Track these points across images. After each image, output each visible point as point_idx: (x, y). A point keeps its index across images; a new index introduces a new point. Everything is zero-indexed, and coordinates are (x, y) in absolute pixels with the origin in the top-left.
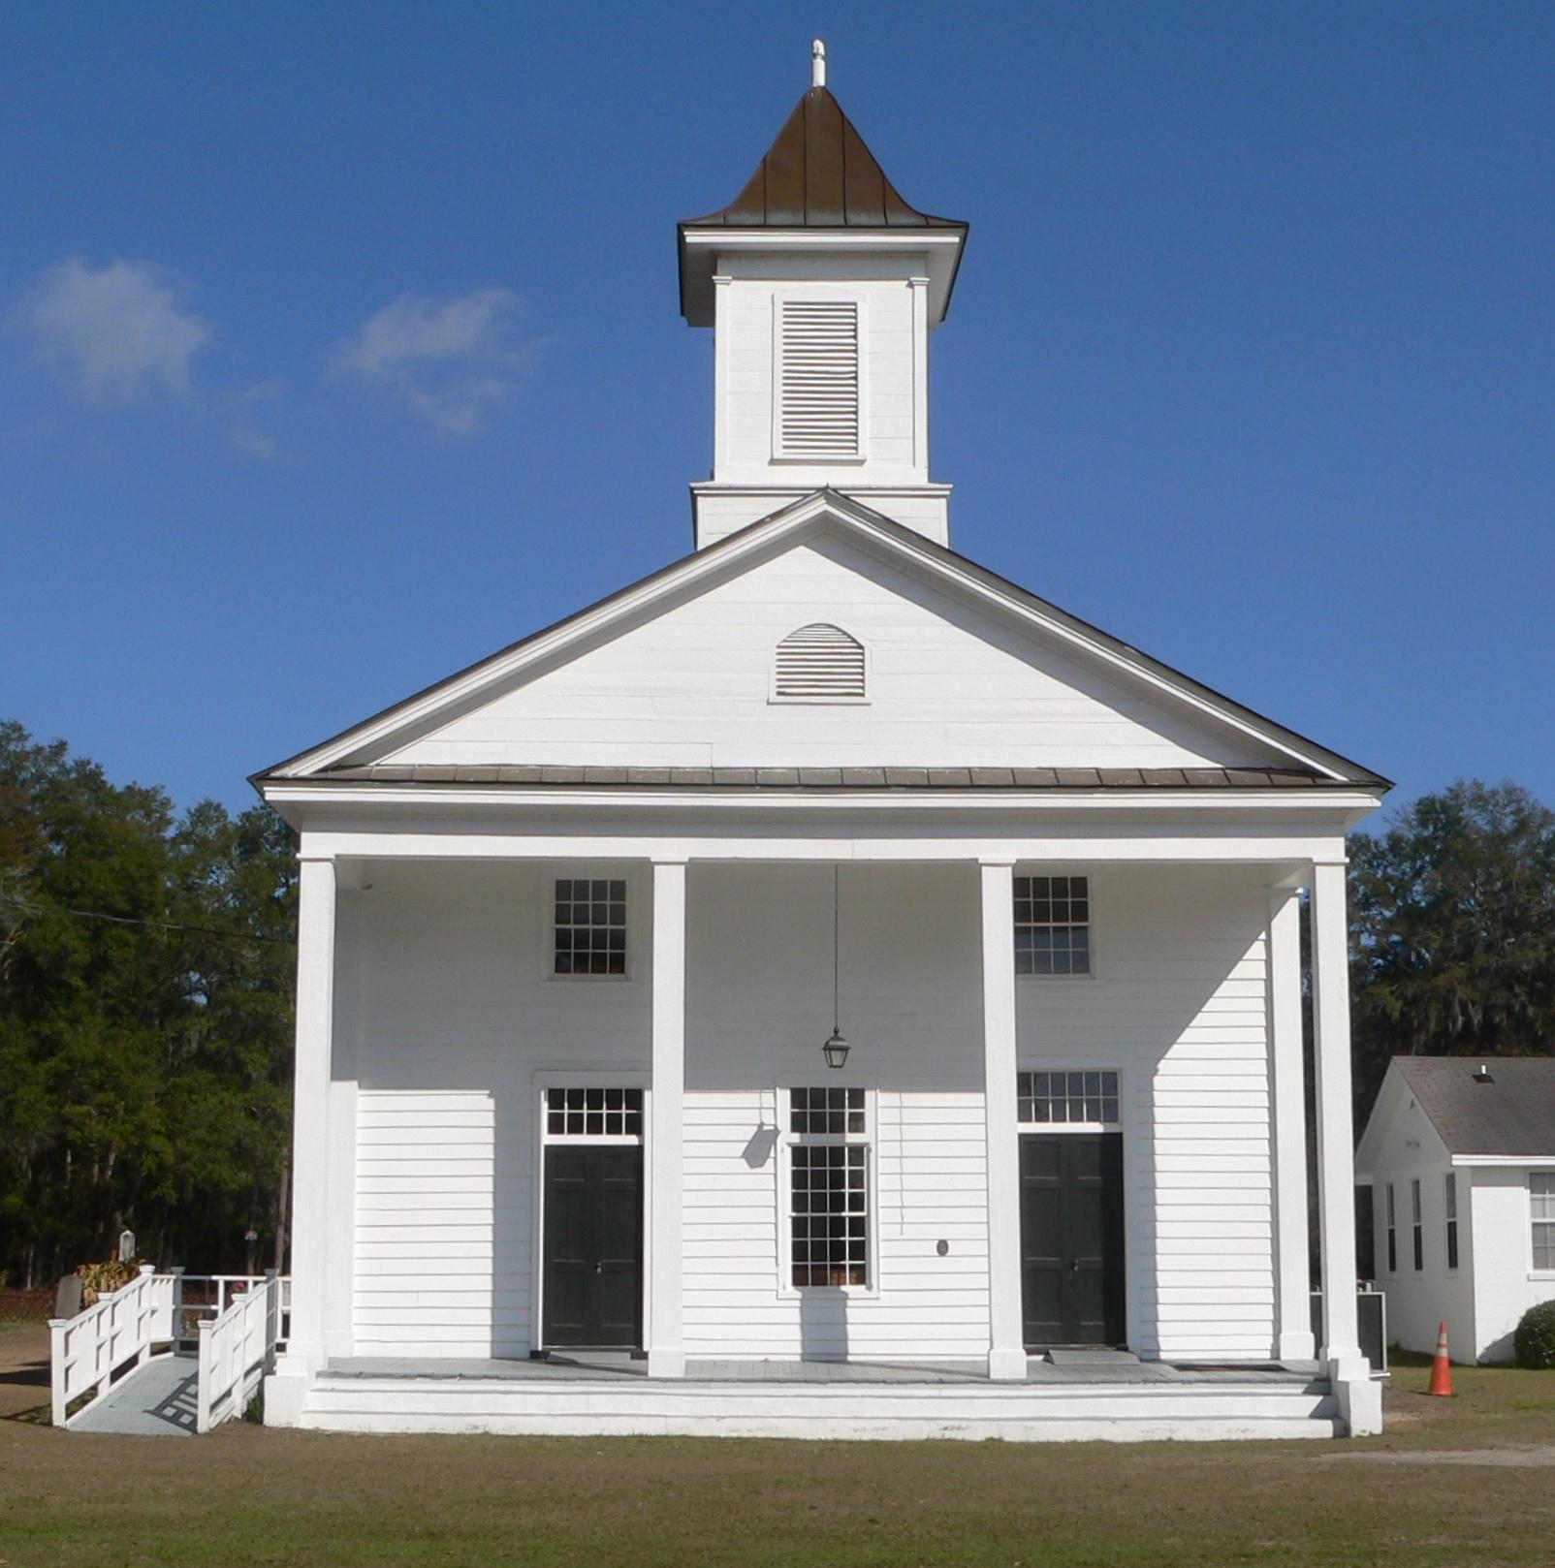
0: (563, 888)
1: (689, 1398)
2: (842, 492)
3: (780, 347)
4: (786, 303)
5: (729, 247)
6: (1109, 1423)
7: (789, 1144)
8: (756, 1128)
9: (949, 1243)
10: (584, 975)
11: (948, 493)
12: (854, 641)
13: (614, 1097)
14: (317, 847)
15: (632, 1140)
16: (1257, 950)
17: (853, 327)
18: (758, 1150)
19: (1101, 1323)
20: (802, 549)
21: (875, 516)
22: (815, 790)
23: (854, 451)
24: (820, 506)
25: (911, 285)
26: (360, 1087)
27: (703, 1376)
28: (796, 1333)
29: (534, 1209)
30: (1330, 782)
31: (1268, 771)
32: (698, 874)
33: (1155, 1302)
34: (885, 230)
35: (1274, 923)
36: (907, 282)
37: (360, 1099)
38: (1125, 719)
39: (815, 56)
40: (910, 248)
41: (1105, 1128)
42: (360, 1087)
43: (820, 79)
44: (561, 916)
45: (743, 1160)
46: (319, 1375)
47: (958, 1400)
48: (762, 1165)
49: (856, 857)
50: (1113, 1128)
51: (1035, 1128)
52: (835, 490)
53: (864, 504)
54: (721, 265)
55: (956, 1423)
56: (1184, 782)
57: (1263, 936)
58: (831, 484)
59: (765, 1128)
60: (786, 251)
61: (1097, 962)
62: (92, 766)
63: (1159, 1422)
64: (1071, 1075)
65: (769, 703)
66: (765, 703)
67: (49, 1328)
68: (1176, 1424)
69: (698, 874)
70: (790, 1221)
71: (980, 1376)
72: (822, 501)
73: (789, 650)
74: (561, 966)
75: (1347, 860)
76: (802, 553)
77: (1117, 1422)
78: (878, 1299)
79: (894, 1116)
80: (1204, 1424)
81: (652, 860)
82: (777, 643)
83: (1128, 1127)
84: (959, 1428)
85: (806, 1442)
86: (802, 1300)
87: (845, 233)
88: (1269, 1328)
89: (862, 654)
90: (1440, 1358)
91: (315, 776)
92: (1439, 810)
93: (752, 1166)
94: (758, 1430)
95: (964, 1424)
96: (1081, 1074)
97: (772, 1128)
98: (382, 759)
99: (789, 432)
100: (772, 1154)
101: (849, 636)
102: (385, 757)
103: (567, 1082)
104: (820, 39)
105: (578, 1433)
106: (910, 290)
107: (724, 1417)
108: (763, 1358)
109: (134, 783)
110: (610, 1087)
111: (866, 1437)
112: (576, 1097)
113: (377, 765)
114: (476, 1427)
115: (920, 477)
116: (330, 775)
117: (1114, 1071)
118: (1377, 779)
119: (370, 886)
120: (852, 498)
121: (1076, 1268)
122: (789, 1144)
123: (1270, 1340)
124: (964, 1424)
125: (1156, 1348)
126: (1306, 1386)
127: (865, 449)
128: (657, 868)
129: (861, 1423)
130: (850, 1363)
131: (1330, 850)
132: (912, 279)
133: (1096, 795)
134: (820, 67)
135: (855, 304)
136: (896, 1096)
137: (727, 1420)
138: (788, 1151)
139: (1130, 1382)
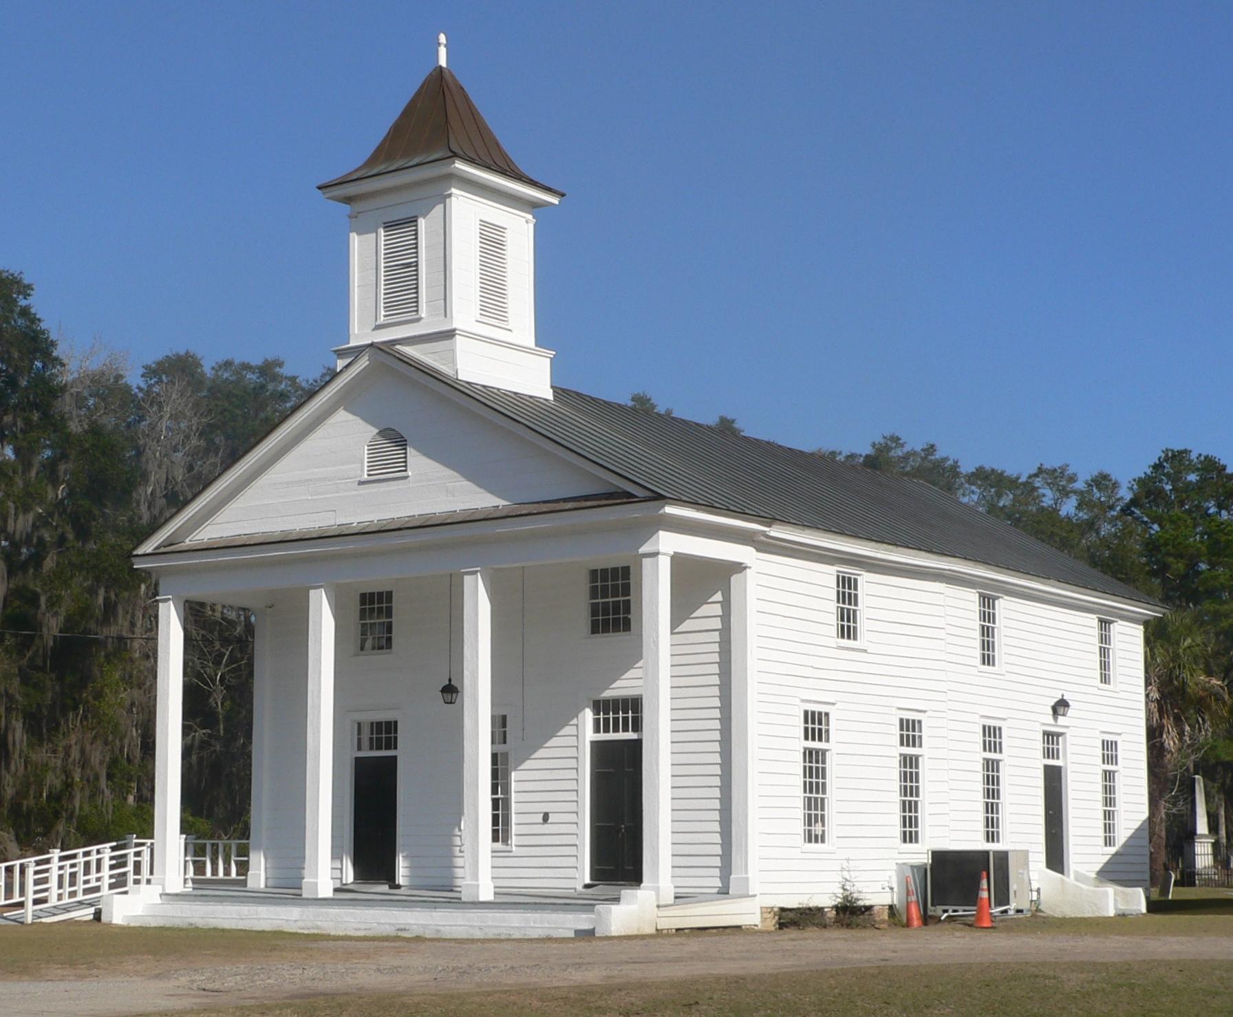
4: (481, 221)
10: (619, 633)
34: (693, 506)
39: (439, 44)
44: (594, 593)
62: (951, 462)
74: (595, 629)
90: (981, 899)
94: (313, 928)
98: (192, 536)
102: (194, 534)
109: (1041, 465)
115: (530, 341)
116: (163, 550)
130: (1039, 898)
134: (443, 52)
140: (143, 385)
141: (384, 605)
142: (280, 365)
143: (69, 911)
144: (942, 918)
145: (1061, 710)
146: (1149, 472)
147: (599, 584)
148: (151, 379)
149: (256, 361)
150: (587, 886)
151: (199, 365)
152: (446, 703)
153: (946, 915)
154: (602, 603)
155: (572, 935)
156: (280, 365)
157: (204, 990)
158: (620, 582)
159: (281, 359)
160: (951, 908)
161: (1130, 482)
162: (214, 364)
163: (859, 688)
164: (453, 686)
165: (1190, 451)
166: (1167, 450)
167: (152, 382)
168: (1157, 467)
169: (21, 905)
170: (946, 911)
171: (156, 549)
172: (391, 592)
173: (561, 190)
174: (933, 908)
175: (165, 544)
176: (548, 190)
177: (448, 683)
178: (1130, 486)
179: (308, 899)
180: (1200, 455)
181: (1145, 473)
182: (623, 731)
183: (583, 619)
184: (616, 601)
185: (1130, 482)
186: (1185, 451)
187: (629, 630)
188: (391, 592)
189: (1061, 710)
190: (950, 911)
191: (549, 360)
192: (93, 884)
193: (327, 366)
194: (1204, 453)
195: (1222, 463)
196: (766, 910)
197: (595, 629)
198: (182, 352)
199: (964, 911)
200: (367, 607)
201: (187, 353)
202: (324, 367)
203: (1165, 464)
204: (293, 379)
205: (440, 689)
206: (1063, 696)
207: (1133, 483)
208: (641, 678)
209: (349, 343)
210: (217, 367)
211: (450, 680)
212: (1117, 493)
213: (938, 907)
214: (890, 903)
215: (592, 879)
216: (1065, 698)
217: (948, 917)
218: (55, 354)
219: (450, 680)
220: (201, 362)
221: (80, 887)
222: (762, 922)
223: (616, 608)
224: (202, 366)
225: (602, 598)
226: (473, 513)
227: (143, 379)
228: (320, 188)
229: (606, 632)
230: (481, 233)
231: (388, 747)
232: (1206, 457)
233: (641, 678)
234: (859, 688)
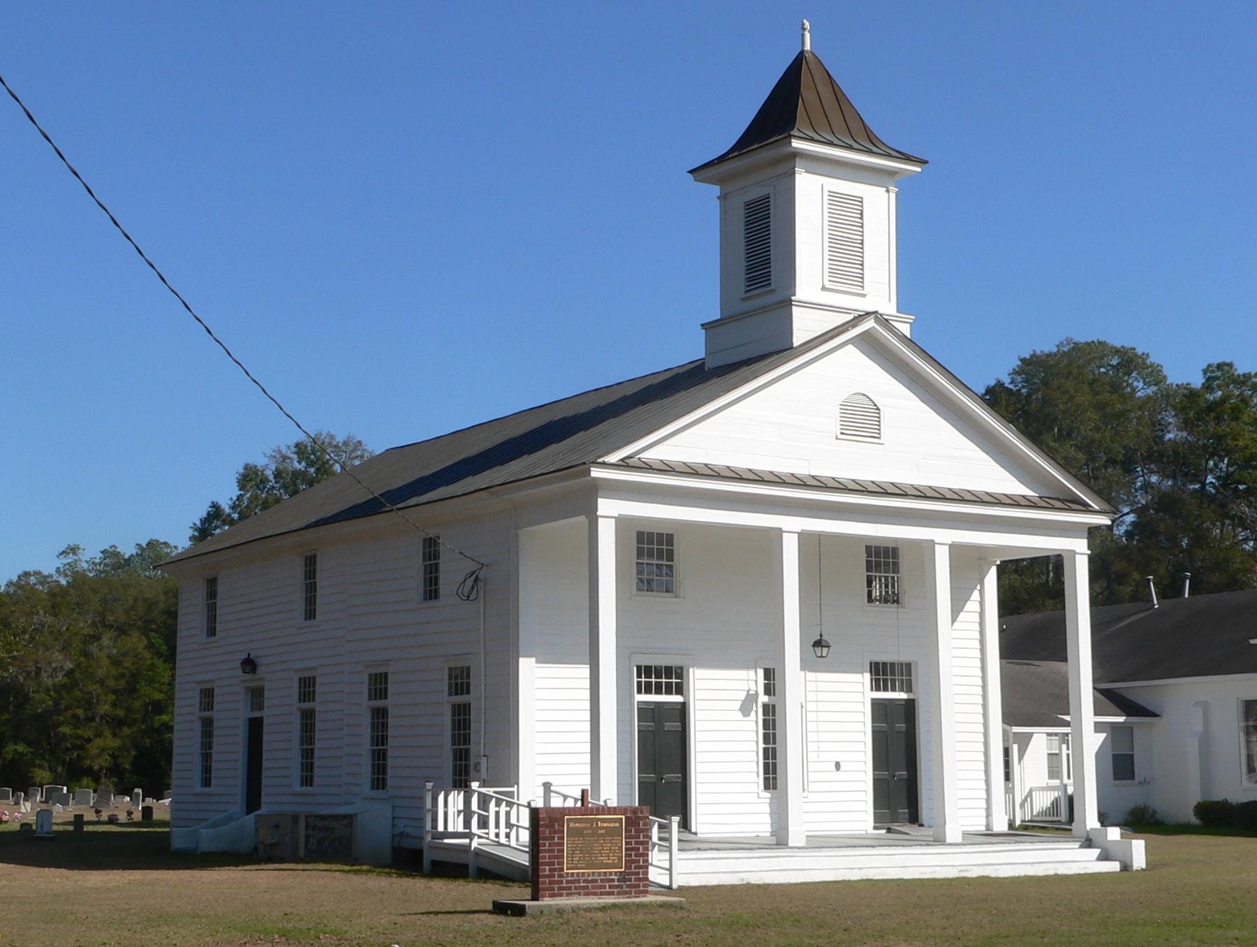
1: (826, 858)
2: (885, 317)
3: (826, 219)
4: (830, 192)
6: (1030, 865)
8: (745, 693)
11: (912, 321)
12: (875, 405)
13: (668, 671)
14: (608, 507)
15: (678, 699)
16: (976, 595)
17: (860, 212)
19: (907, 811)
21: (900, 333)
22: (727, 479)
23: (861, 288)
24: (869, 324)
25: (888, 191)
26: (537, 662)
27: (818, 843)
28: (768, 819)
29: (632, 744)
30: (1091, 509)
31: (1062, 501)
32: (805, 538)
35: (986, 580)
36: (885, 189)
40: (888, 169)
45: (740, 712)
47: (949, 855)
48: (749, 715)
49: (879, 535)
50: (912, 696)
52: (881, 315)
54: (798, 161)
55: (965, 868)
56: (1014, 502)
57: (978, 587)
58: (880, 312)
59: (751, 692)
61: (906, 598)
63: (1050, 864)
64: (891, 663)
65: (837, 438)
66: (834, 438)
69: (805, 538)
75: (1089, 552)
76: (850, 347)
77: (1034, 865)
78: (807, 797)
80: (1069, 865)
82: (843, 400)
83: (920, 695)
86: (770, 799)
88: (984, 813)
89: (879, 413)
91: (618, 463)
92: (310, 452)
93: (744, 716)
95: (969, 868)
97: (754, 692)
100: (754, 709)
101: (873, 402)
103: (644, 663)
105: (793, 881)
106: (887, 194)
107: (862, 868)
108: (755, 834)
111: (974, 873)
114: (743, 880)
117: (909, 662)
120: (890, 322)
121: (896, 778)
123: (985, 820)
124: (969, 868)
126: (1080, 843)
129: (925, 870)
131: (1080, 546)
132: (890, 188)
133: (995, 508)
135: (862, 198)
137: (864, 870)
139: (1031, 842)
143: (1021, 808)
152: (818, 657)
155: (490, 907)
176: (907, 158)
177: (819, 638)
179: (951, 844)
191: (908, 325)
208: (953, 638)
211: (821, 636)
219: (821, 636)
228: (690, 172)
233: (953, 638)
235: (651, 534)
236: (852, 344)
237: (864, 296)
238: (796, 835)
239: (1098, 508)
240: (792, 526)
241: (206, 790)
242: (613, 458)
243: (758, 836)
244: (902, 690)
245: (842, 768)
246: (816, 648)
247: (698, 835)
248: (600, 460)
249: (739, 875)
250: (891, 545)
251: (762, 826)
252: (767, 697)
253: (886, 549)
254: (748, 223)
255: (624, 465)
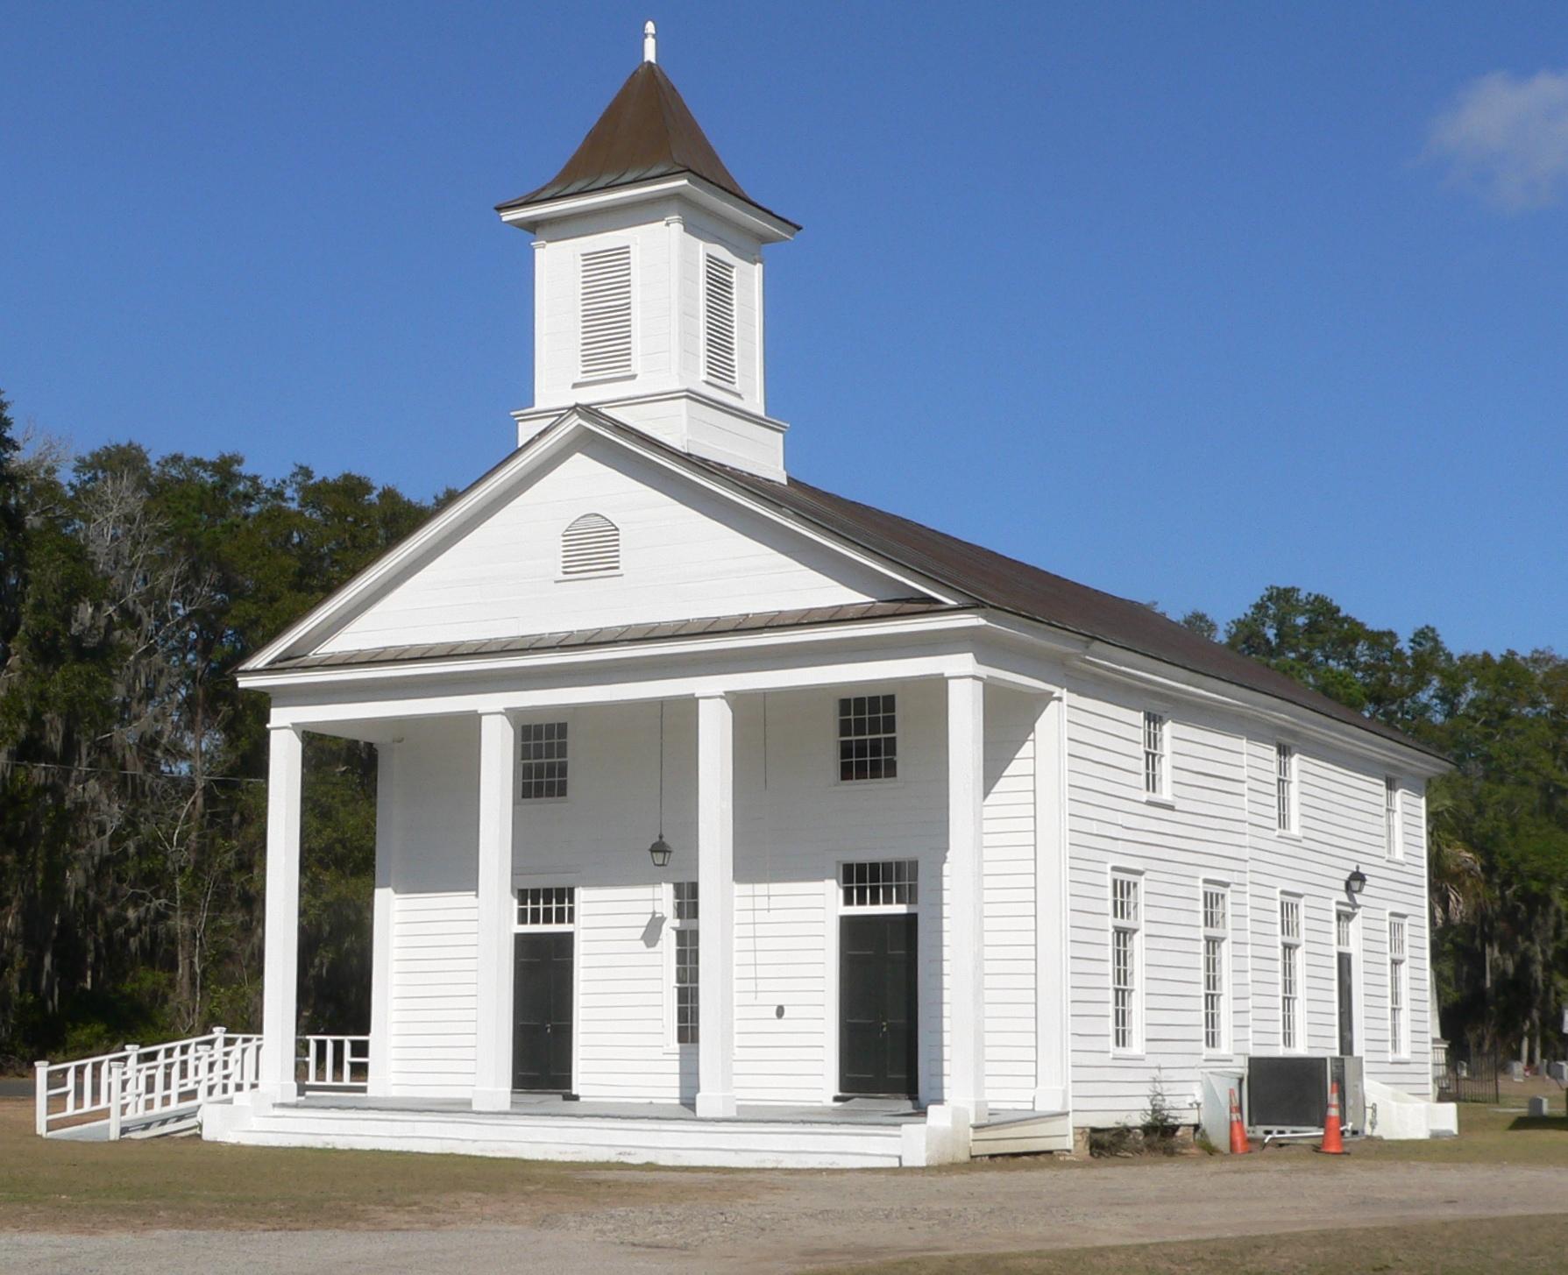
0: (845, 705)
4: (583, 255)
5: (542, 217)
6: (733, 1153)
7: (674, 929)
8: (650, 916)
9: (785, 1008)
12: (613, 525)
14: (282, 719)
18: (651, 934)
20: (578, 456)
24: (575, 421)
33: (941, 1060)
37: (397, 901)
38: (803, 567)
39: (646, 36)
41: (908, 908)
42: (396, 892)
43: (650, 54)
44: (845, 729)
46: (274, 1105)
48: (654, 945)
50: (913, 911)
51: (856, 910)
53: (545, 420)
55: (628, 1150)
60: (589, 212)
64: (858, 865)
67: (35, 1068)
68: (781, 1157)
69: (737, 701)
70: (676, 990)
71: (459, 1108)
72: (575, 417)
73: (569, 535)
74: (846, 773)
79: (748, 903)
81: (696, 695)
83: (920, 909)
84: (629, 1154)
85: (295, 1148)
87: (609, 192)
90: (1331, 1118)
95: (633, 1150)
96: (891, 863)
99: (587, 360)
104: (654, 22)
107: (476, 1141)
108: (648, 1101)
110: (558, 886)
111: (318, 1143)
112: (535, 895)
113: (314, 654)
114: (328, 1144)
118: (975, 601)
119: (400, 741)
122: (674, 929)
124: (633, 1150)
125: (939, 1098)
127: (637, 366)
128: (951, 682)
136: (749, 886)
138: (674, 934)
140: (75, 481)
141: (556, 741)
142: (240, 462)
144: (1266, 1141)
145: (1356, 885)
146: (1249, 613)
147: (852, 717)
148: (84, 474)
149: (211, 456)
150: (836, 1099)
151: (145, 459)
153: (1270, 1136)
154: (857, 741)
156: (240, 462)
157: (634, 1245)
158: (881, 715)
159: (241, 455)
160: (1275, 1129)
161: (1228, 624)
162: (159, 459)
163: (1165, 854)
164: (664, 843)
165: (1299, 590)
166: (1271, 587)
167: (86, 478)
168: (1260, 607)
169: (105, 1114)
170: (1268, 1132)
171: (269, 663)
172: (566, 724)
173: (798, 223)
174: (1251, 1128)
175: (281, 658)
177: (658, 839)
178: (1228, 628)
179: (479, 1113)
180: (1310, 594)
181: (1246, 615)
182: (885, 903)
183: (831, 760)
184: (889, 738)
185: (1228, 624)
186: (1293, 590)
187: (894, 775)
188: (566, 724)
189: (1356, 885)
190: (1275, 1132)
192: (191, 1086)
193: (299, 464)
194: (1315, 592)
195: (1334, 603)
196: (1079, 1130)
197: (846, 773)
198: (124, 443)
199: (1293, 1132)
200: (532, 743)
201: (130, 444)
202: (296, 465)
203: (1269, 604)
204: (254, 479)
205: (650, 847)
206: (1358, 867)
207: (1232, 625)
209: (532, 405)
210: (162, 462)
211: (661, 837)
212: (1214, 637)
213: (1258, 1127)
214: (1197, 1122)
215: (841, 1090)
216: (1361, 870)
217: (1271, 1139)
218: (8, 434)
219: (661, 837)
220: (148, 456)
221: (174, 1092)
222: (1075, 1145)
223: (876, 750)
224: (148, 460)
225: (856, 735)
226: (870, 608)
227: (75, 474)
229: (890, 776)
230: (708, 272)
231: (560, 920)
232: (1317, 597)
234: (1165, 854)
235: (538, 728)
236: (579, 451)
237: (633, 377)
238: (706, 1103)
239: (955, 603)
240: (710, 688)
241: (1121, 1051)
242: (261, 660)
243: (651, 1103)
244: (899, 901)
245: (785, 1016)
246: (654, 854)
247: (581, 1099)
248: (241, 668)
249: (324, 1137)
250: (881, 692)
251: (669, 1093)
252: (678, 921)
253: (874, 700)
254: (587, 316)
255: (270, 669)
